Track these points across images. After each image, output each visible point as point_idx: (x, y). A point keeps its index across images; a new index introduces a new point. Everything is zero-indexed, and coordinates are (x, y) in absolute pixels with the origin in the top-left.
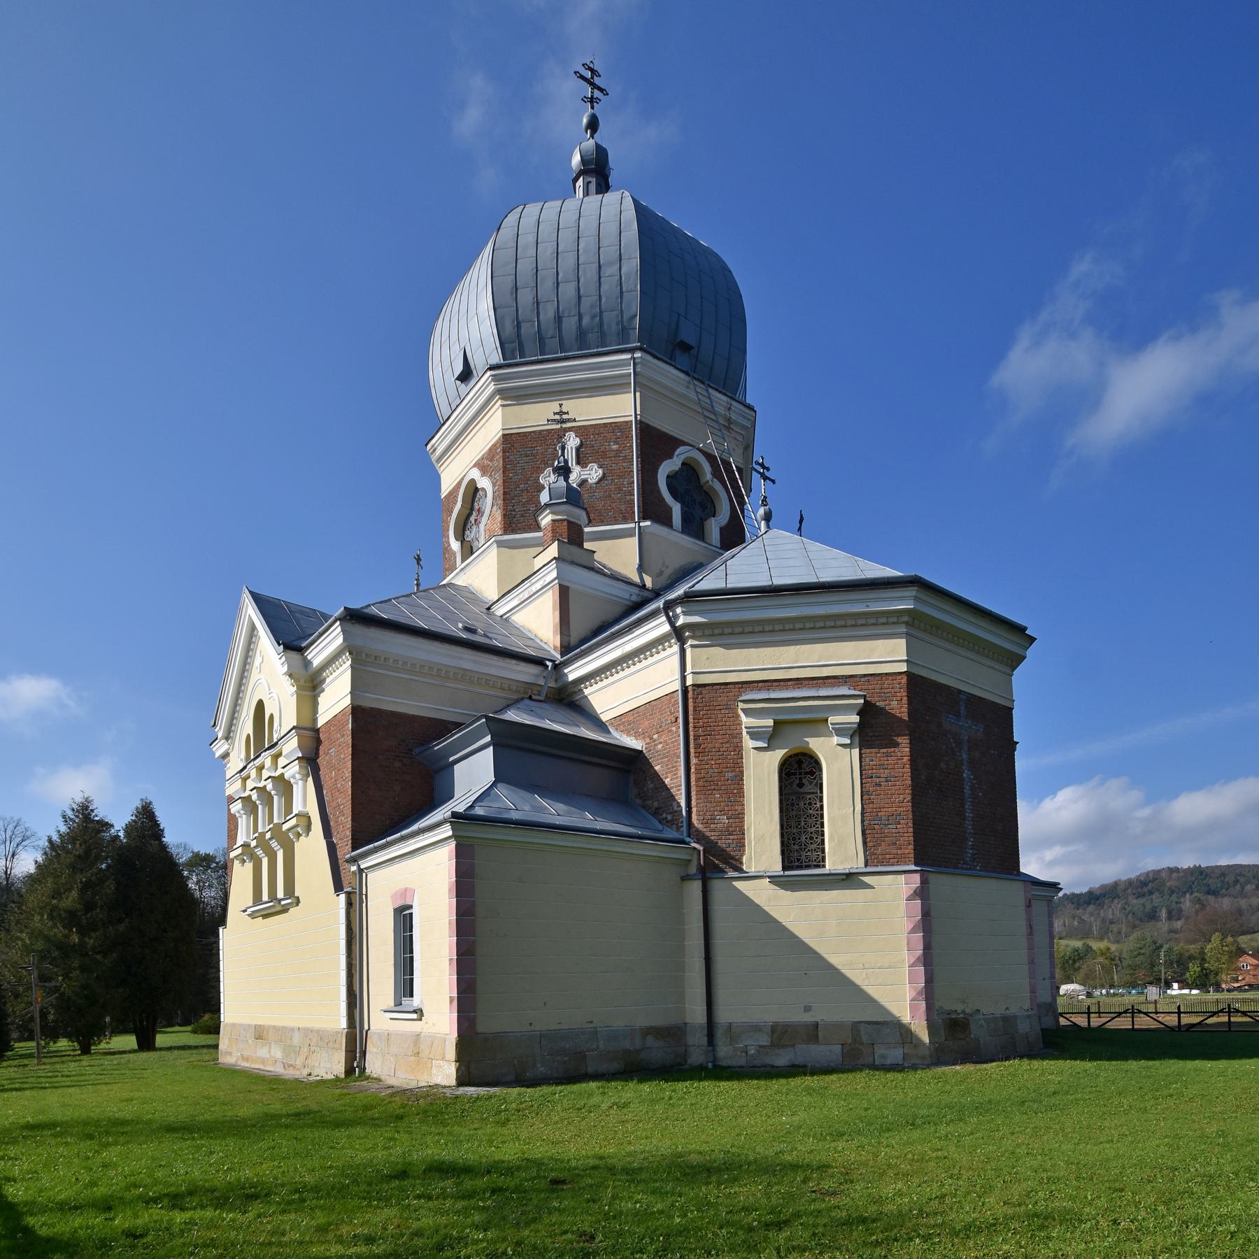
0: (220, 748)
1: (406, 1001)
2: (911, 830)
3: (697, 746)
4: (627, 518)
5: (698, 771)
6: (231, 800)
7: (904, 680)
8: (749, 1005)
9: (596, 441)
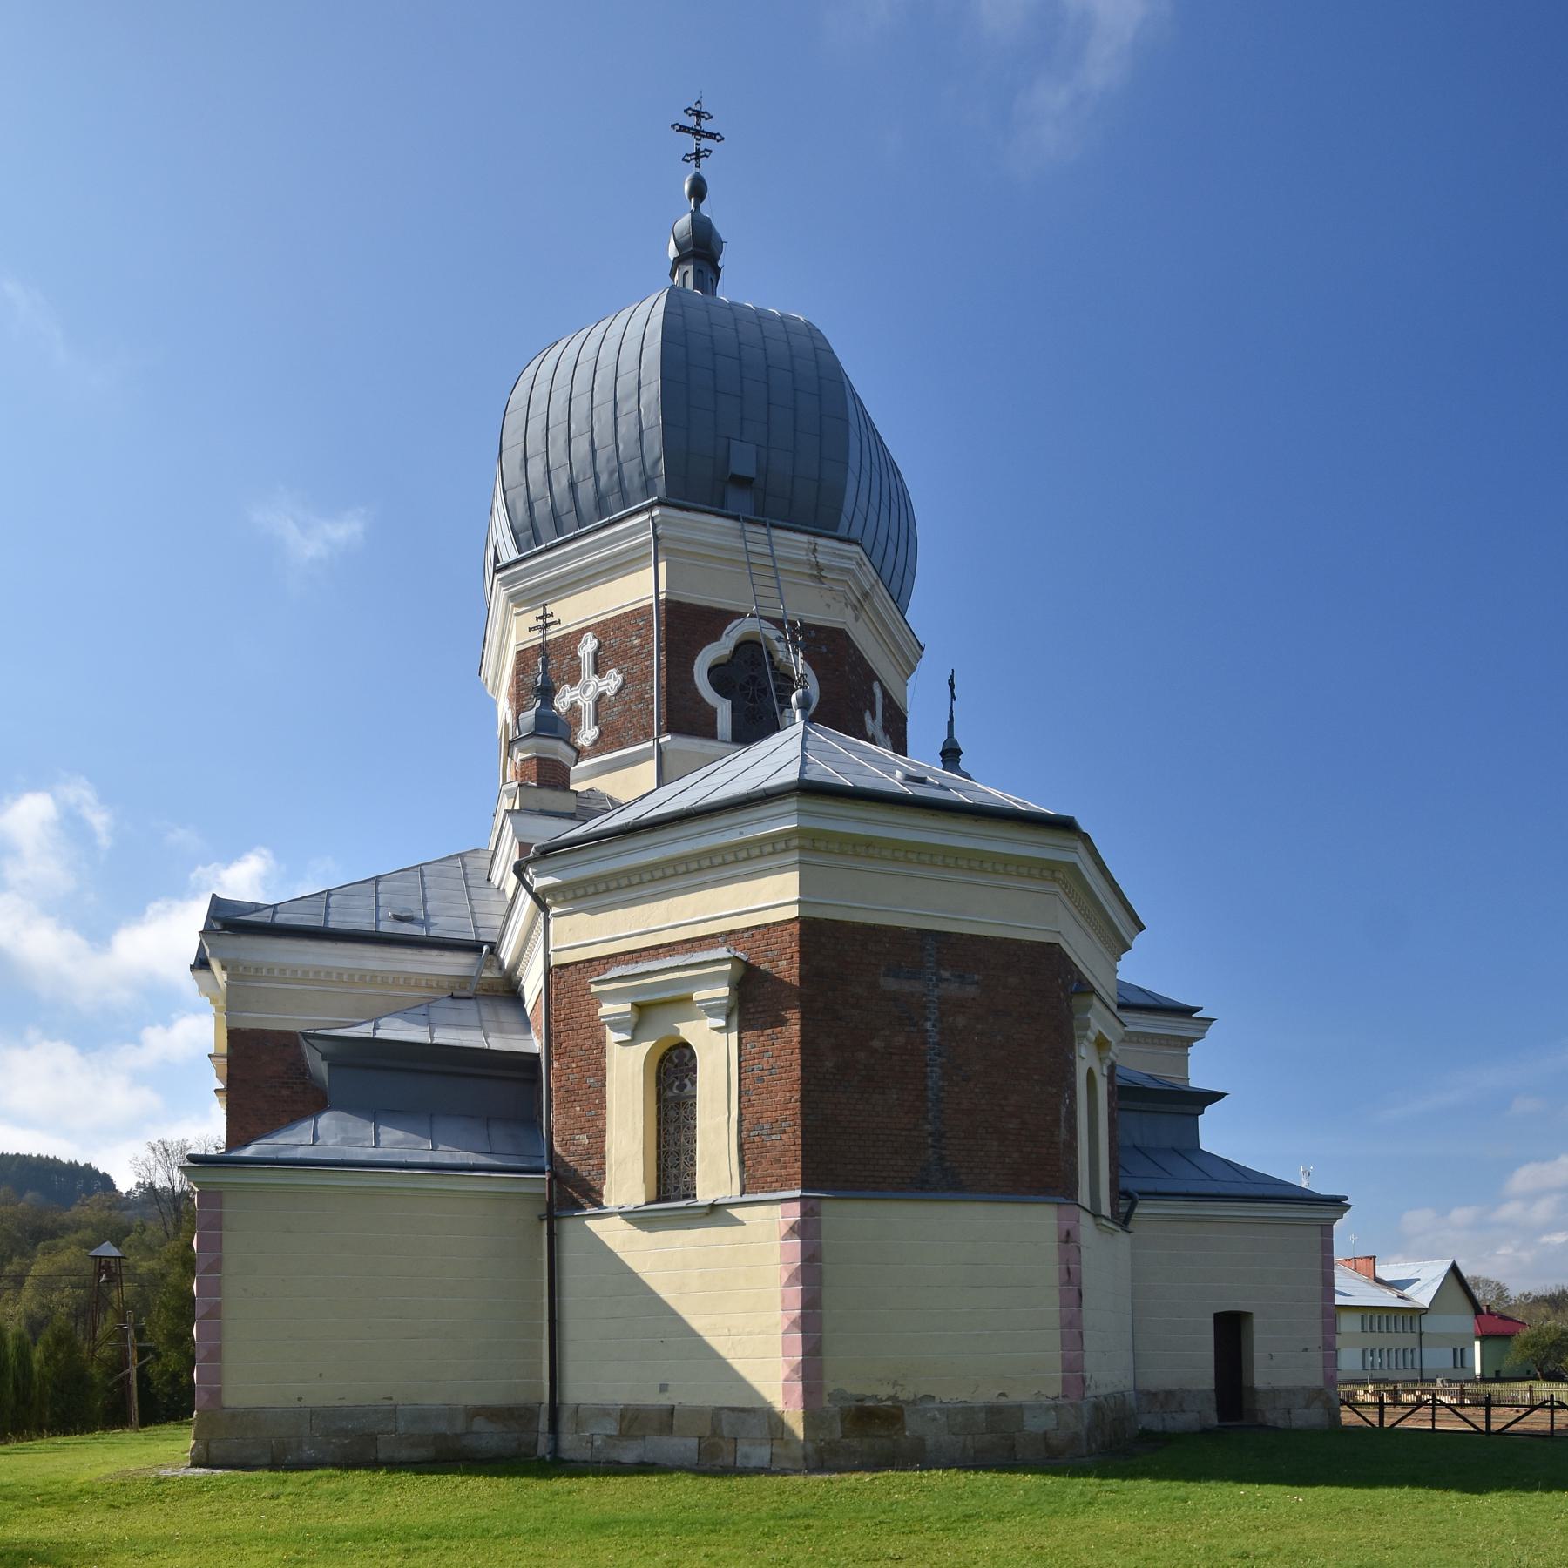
2: (799, 1141)
9: (614, 637)
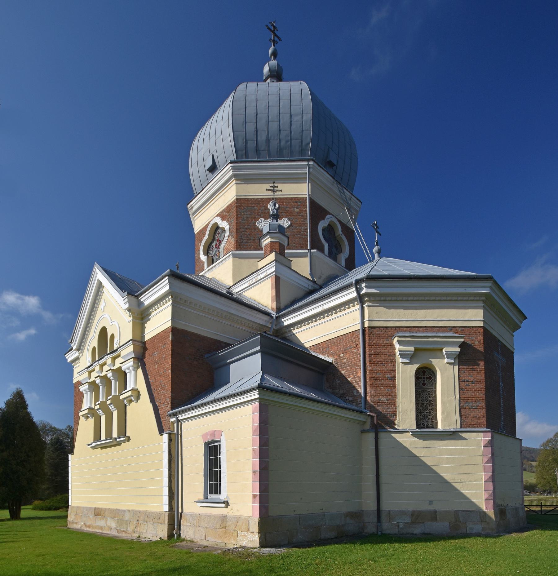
0: (70, 357)
1: (212, 497)
3: (371, 360)
4: (304, 247)
5: (371, 374)
6: (80, 383)
7: (482, 331)
8: (400, 500)
9: (286, 206)
